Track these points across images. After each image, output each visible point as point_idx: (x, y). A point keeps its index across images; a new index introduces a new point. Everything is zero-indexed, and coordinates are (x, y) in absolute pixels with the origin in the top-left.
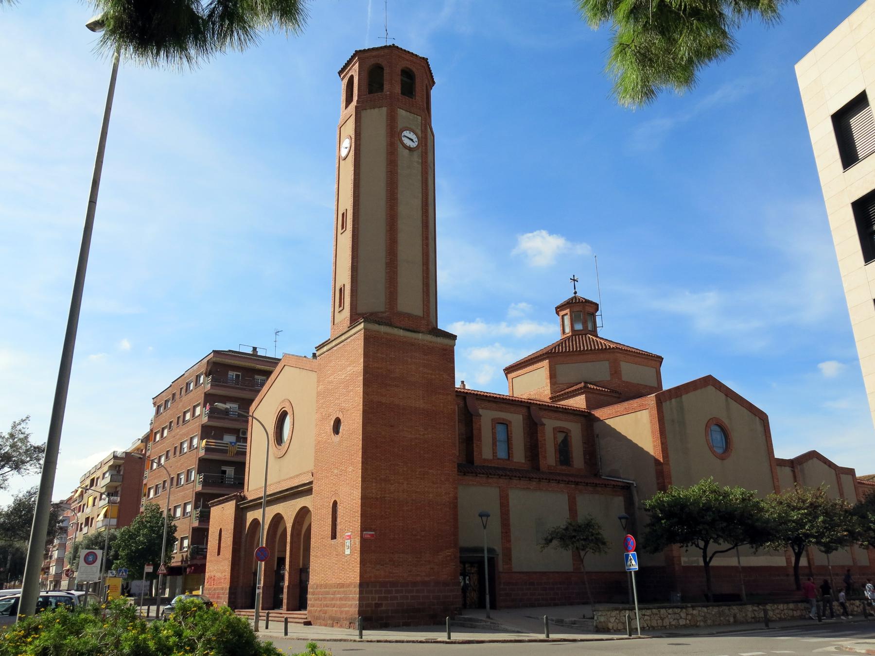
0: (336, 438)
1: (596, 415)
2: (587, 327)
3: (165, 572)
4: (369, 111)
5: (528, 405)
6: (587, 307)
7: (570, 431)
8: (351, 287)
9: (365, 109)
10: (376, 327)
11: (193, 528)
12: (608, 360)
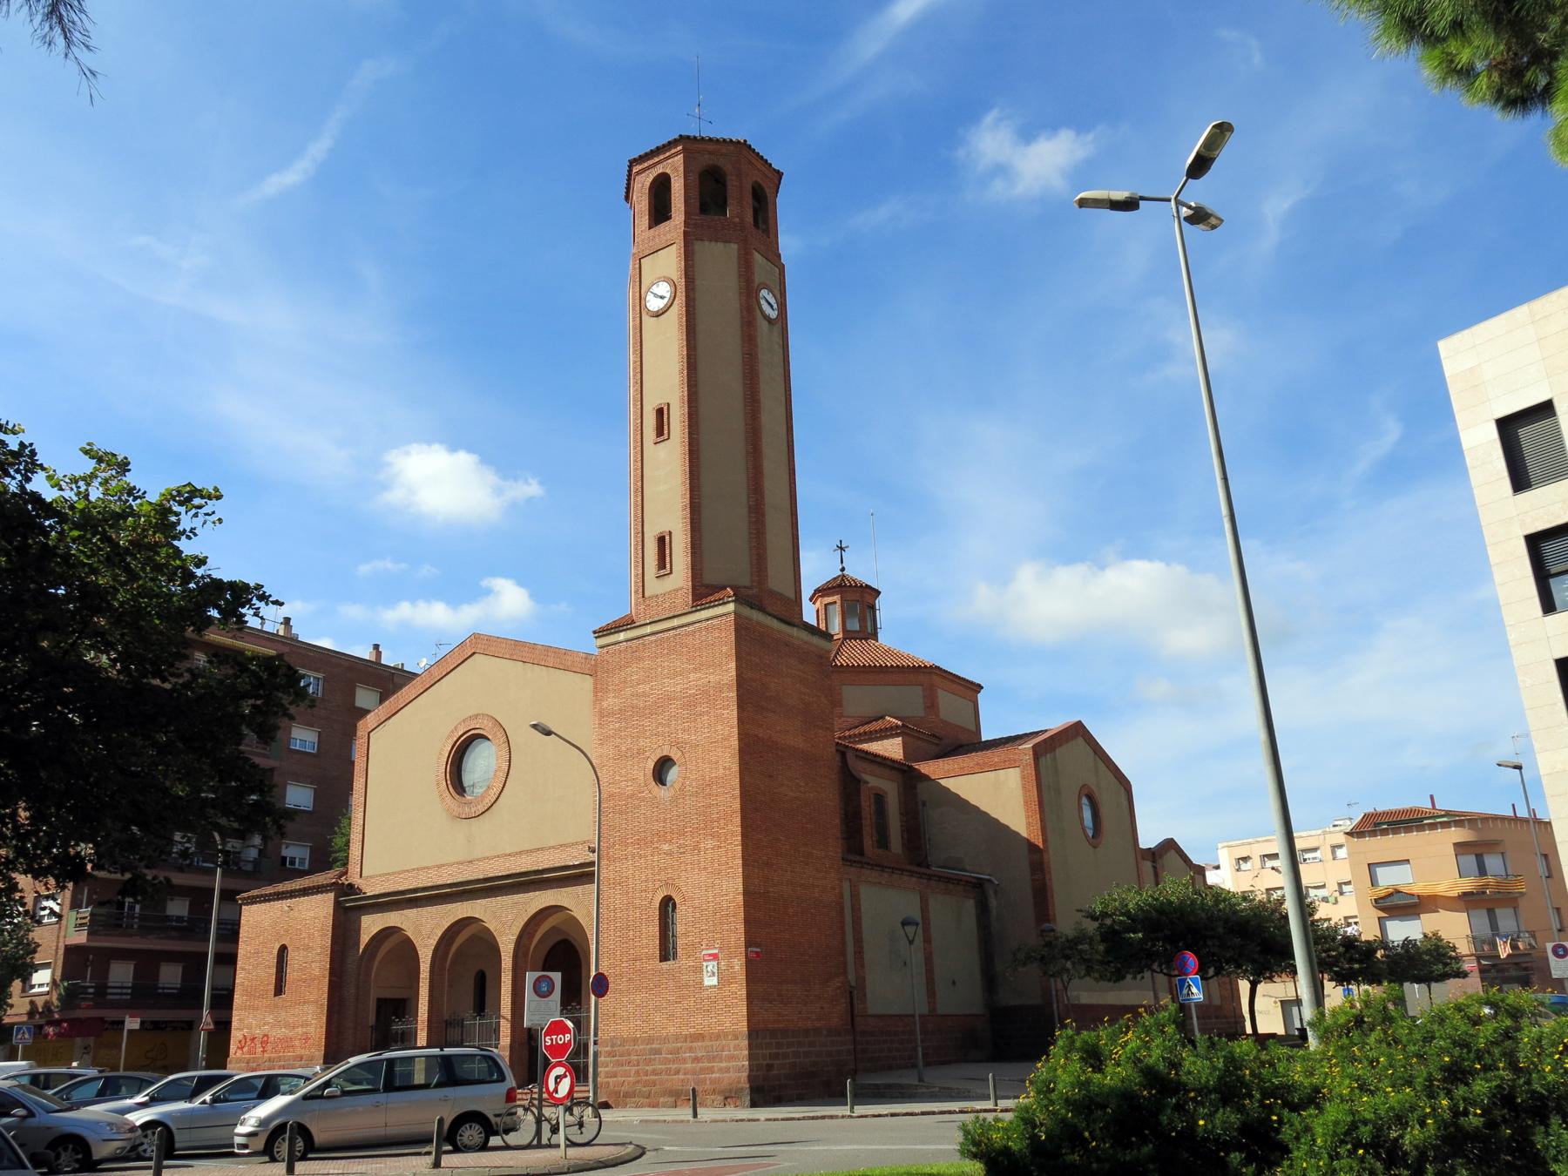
1: (923, 771)
2: (866, 627)
3: (212, 1027)
4: (706, 243)
5: (843, 749)
6: (866, 595)
7: (886, 793)
9: (701, 240)
10: (756, 616)
11: (66, 946)
12: (922, 685)
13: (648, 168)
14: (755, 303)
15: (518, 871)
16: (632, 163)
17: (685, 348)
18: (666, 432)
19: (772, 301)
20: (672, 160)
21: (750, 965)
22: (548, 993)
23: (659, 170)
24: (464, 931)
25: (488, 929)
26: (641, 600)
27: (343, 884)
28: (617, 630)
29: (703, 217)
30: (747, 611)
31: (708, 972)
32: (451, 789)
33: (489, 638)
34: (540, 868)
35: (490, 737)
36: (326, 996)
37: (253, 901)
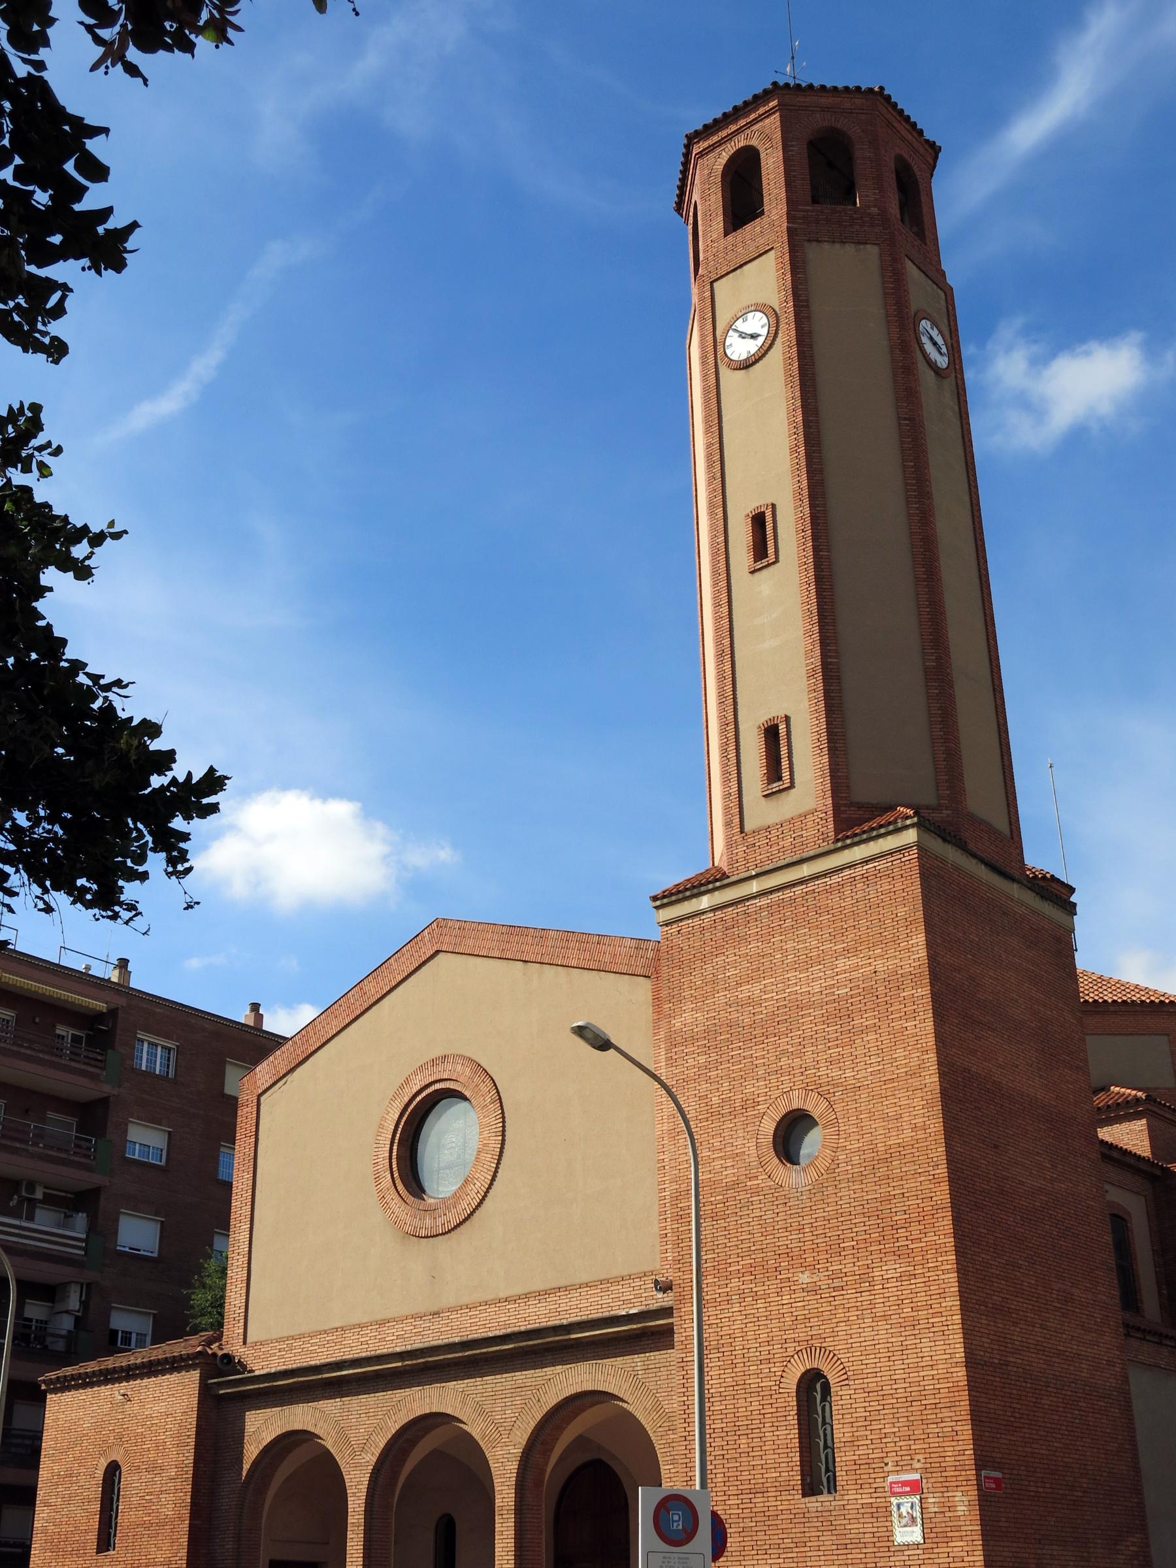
0: (792, 1177)
4: (826, 246)
8: (829, 723)
9: (818, 241)
10: (952, 855)
12: (1168, 1035)
13: (720, 143)
14: (913, 335)
15: (523, 1329)
16: (693, 138)
17: (799, 412)
18: (771, 550)
19: (940, 340)
20: (760, 124)
21: (986, 1503)
22: (683, 1536)
23: (740, 142)
24: (425, 1439)
25: (468, 1437)
26: (738, 837)
27: (214, 1355)
28: (695, 891)
29: (818, 207)
30: (936, 845)
31: (900, 1516)
32: (400, 1187)
33: (463, 926)
34: (565, 1322)
35: (467, 1094)
36: (183, 1553)
37: (65, 1385)
